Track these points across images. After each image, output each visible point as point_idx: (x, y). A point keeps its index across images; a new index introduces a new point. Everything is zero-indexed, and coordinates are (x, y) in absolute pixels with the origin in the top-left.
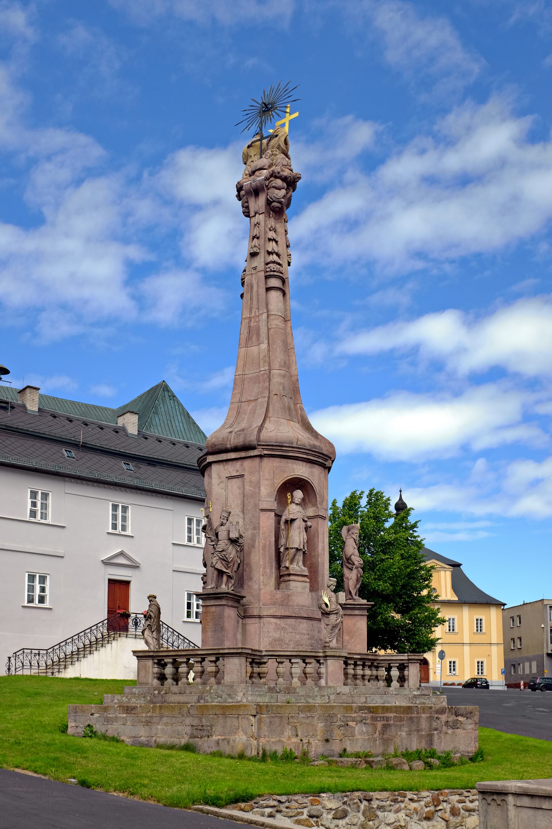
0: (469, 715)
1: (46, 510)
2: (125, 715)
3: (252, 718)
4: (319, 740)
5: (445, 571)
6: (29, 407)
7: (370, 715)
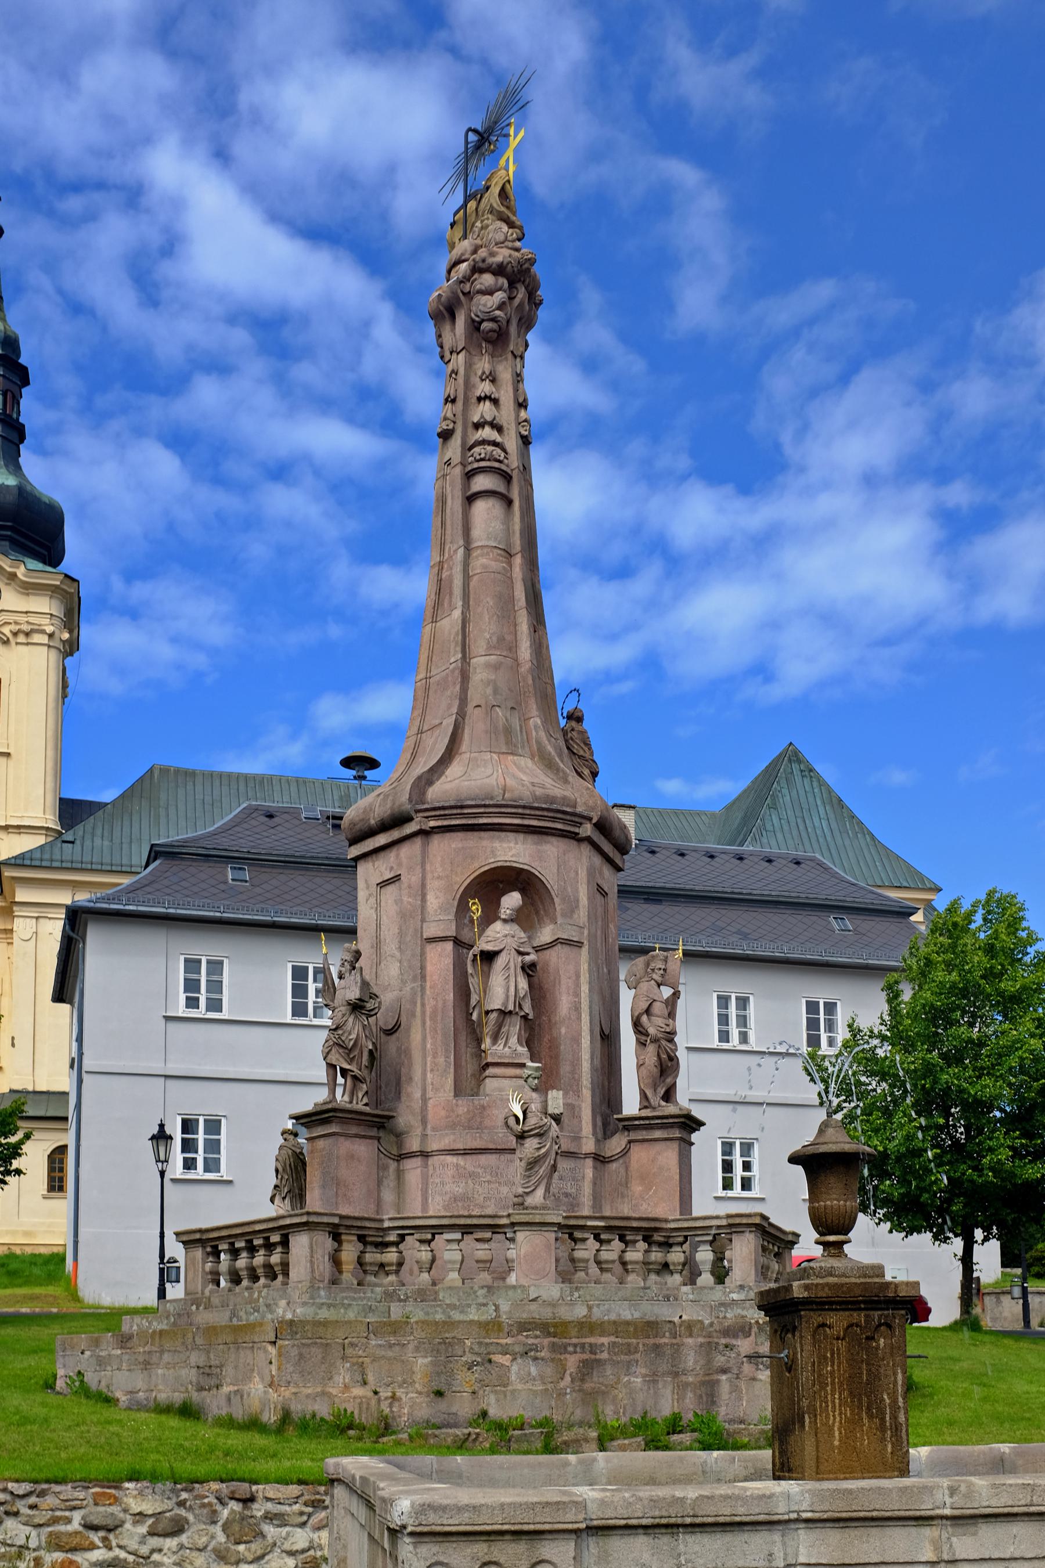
2: (119, 1352)
3: (270, 1348)
4: (420, 1393)
7: (546, 1341)
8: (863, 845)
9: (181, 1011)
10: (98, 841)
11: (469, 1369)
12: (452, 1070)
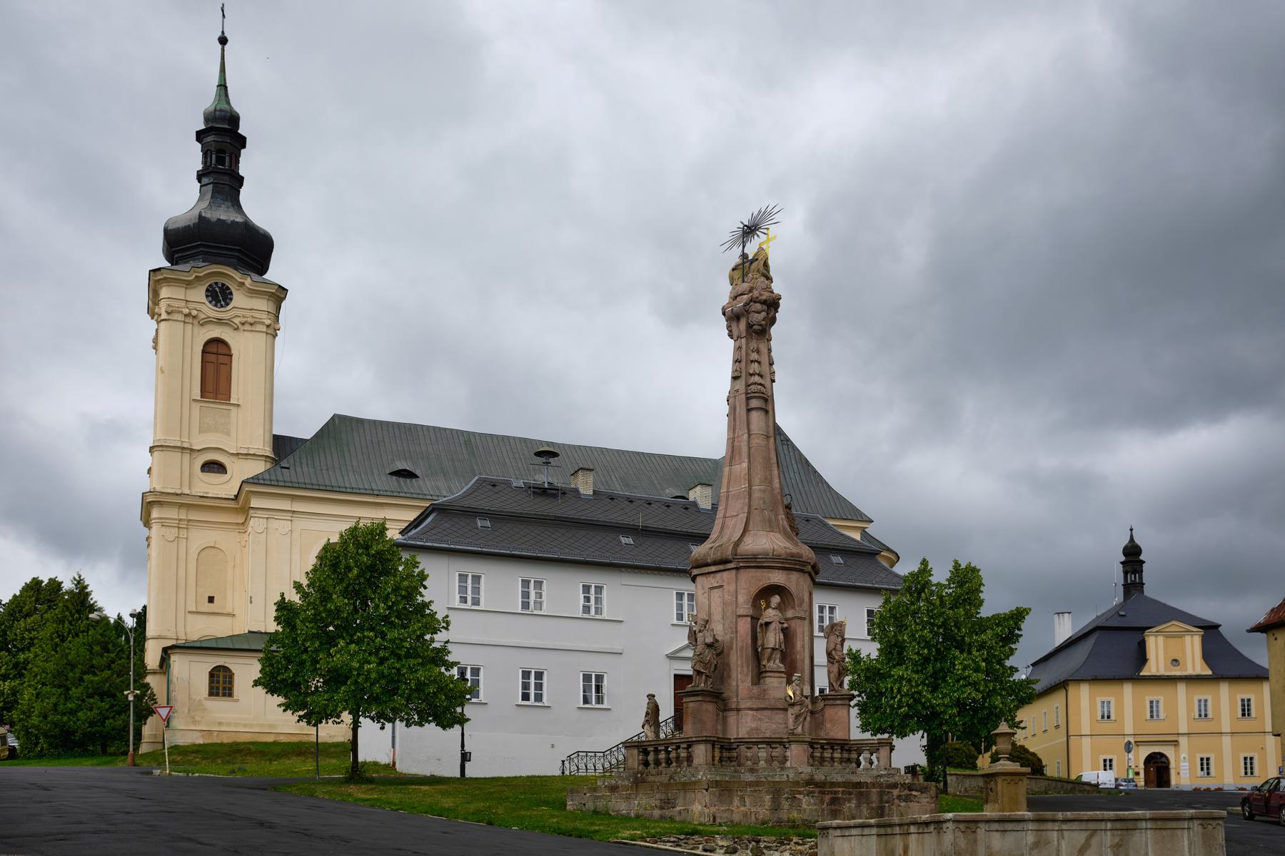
0: (923, 790)
1: (601, 604)
5: (1192, 636)
6: (582, 491)
10: (305, 469)
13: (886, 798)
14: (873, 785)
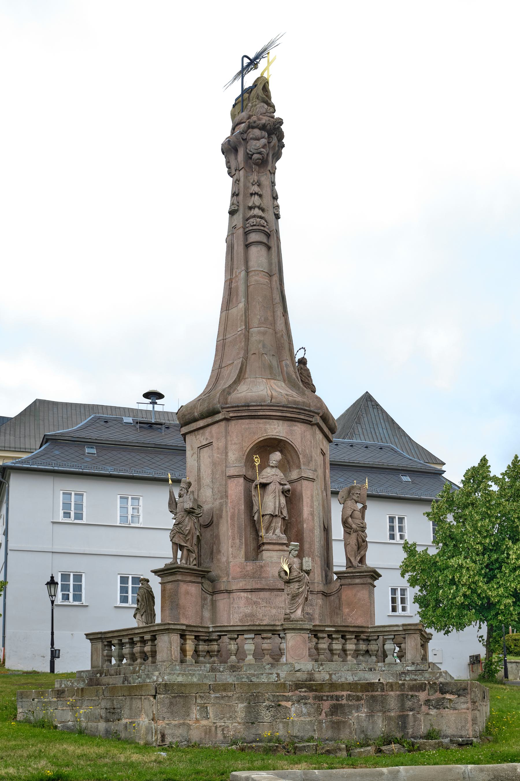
0: (461, 692)
4: (239, 723)
8: (405, 441)
9: (61, 519)
10: (7, 437)
11: (267, 710)
12: (244, 547)
13: (409, 704)
14: (391, 686)
